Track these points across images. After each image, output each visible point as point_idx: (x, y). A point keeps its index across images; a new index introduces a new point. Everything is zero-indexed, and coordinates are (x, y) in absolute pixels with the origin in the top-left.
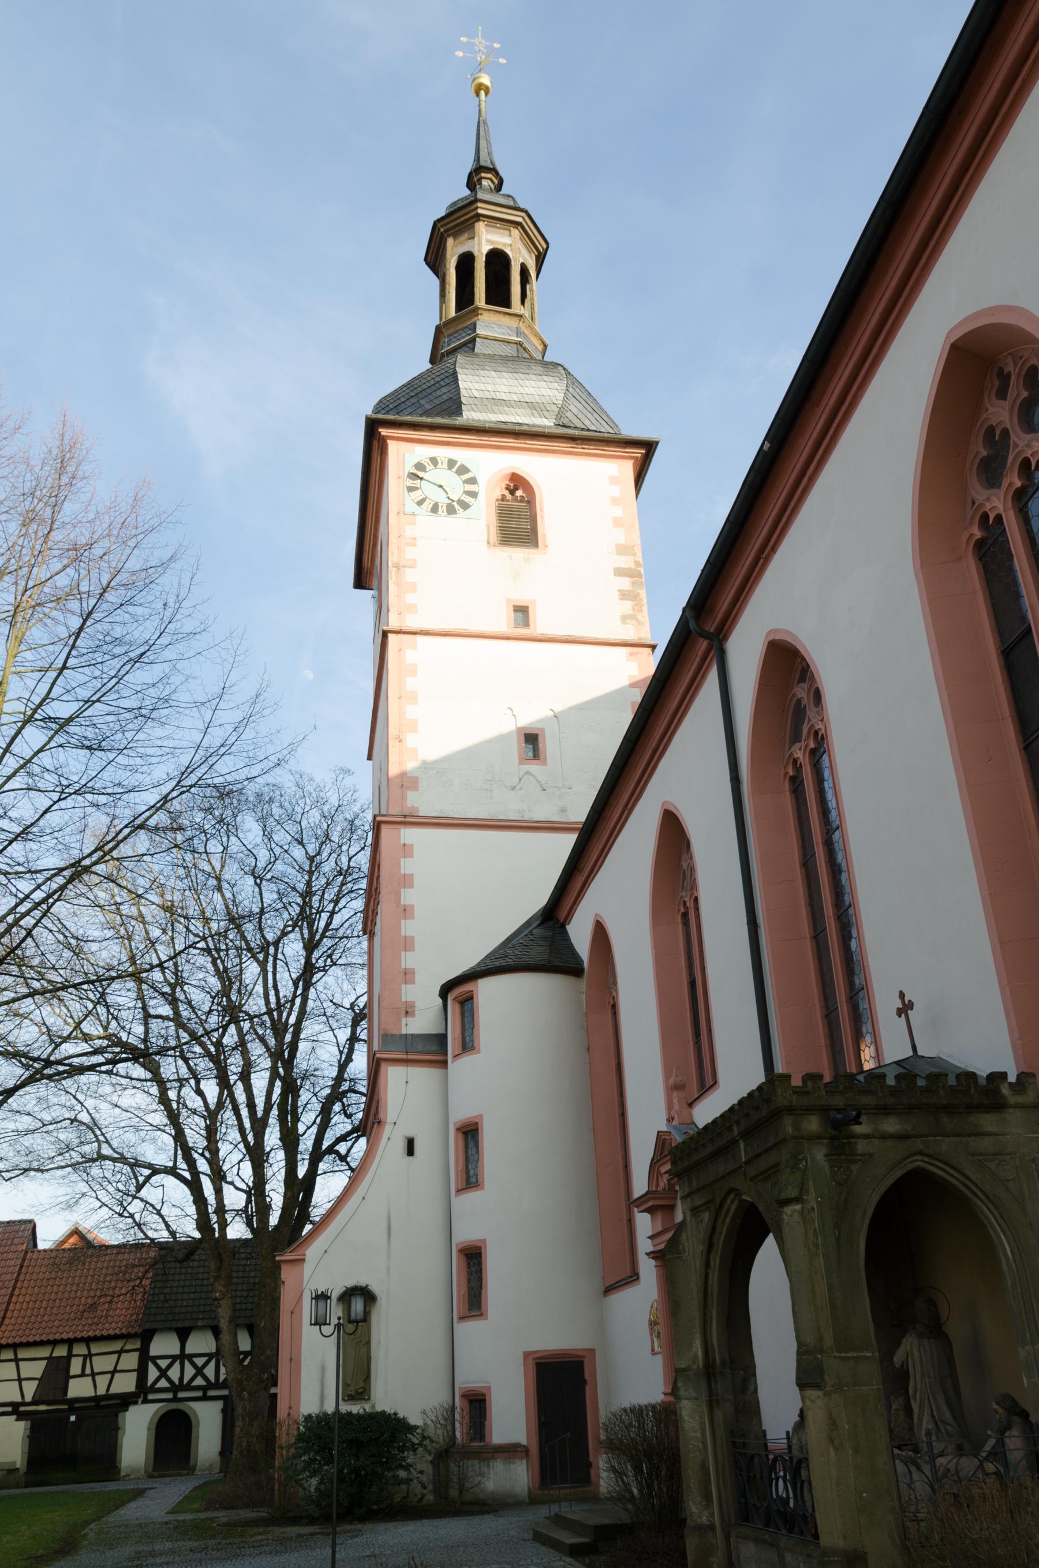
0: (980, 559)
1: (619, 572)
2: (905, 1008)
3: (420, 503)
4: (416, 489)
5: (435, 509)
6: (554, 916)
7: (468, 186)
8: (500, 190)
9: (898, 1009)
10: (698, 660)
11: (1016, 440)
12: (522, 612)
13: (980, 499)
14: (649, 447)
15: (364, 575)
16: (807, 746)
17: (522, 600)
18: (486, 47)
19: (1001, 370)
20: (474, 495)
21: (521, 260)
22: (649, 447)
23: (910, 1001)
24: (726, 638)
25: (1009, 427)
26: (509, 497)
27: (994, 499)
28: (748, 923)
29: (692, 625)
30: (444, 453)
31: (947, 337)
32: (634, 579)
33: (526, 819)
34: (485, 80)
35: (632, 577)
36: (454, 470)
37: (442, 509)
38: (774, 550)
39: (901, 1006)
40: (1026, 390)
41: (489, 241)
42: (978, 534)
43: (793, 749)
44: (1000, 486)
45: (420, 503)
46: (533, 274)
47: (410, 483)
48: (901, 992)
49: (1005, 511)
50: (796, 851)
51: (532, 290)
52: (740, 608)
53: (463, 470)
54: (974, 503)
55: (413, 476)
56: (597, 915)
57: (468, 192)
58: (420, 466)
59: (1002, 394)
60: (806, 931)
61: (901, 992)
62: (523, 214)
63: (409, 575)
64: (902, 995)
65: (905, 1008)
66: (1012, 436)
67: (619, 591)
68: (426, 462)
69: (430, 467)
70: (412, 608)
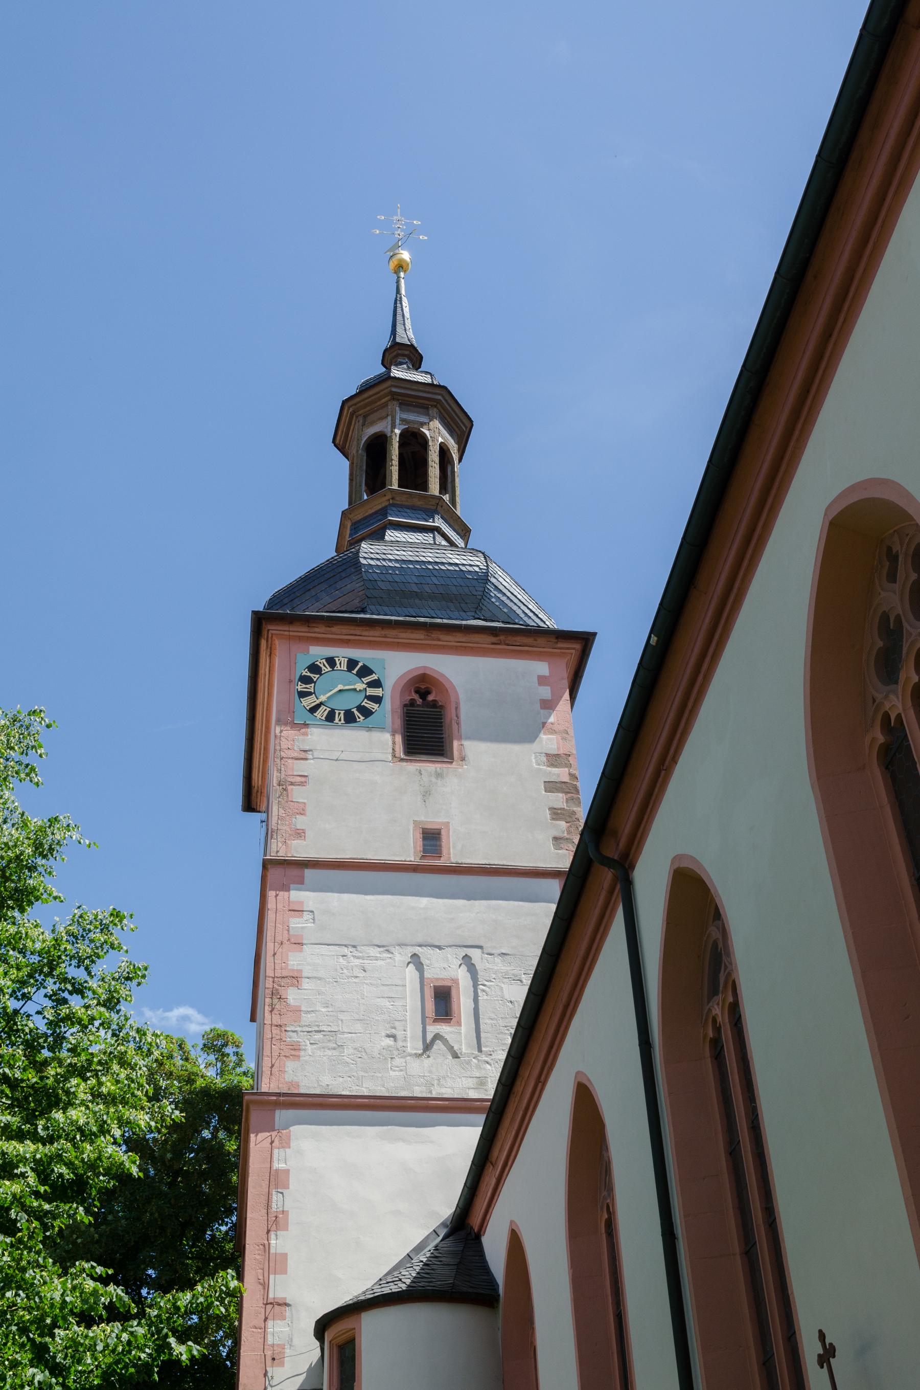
0: (887, 768)
1: (551, 786)
2: (827, 1355)
3: (313, 710)
4: (310, 694)
5: (330, 717)
6: (464, 1229)
7: (383, 364)
8: (420, 367)
9: (819, 1356)
10: (603, 894)
11: (909, 628)
12: (432, 838)
13: (879, 697)
14: (585, 641)
15: (254, 794)
16: (724, 1000)
17: (433, 820)
18: (406, 224)
19: (890, 549)
20: (377, 700)
21: (440, 440)
22: (585, 641)
23: (831, 1344)
24: (632, 867)
25: (901, 613)
26: (419, 701)
27: (892, 697)
28: (663, 1235)
29: (591, 852)
30: (343, 654)
31: (825, 514)
32: (569, 795)
33: (434, 1095)
34: (405, 255)
35: (567, 793)
36: (355, 672)
37: (339, 717)
38: (675, 760)
39: (822, 1352)
40: (915, 571)
41: (403, 421)
42: (881, 739)
43: (711, 1004)
44: (896, 683)
45: (313, 710)
46: (455, 457)
47: (301, 687)
48: (820, 1332)
49: (904, 710)
50: (720, 1137)
51: (453, 472)
52: (642, 833)
53: (365, 671)
54: (874, 701)
55: (305, 680)
56: (512, 1222)
57: (384, 369)
58: (314, 668)
59: (892, 577)
60: (736, 1246)
61: (820, 1332)
62: (444, 393)
63: (297, 794)
64: (822, 1336)
65: (827, 1355)
66: (905, 624)
67: (550, 809)
68: (322, 663)
69: (326, 668)
70: (300, 834)
